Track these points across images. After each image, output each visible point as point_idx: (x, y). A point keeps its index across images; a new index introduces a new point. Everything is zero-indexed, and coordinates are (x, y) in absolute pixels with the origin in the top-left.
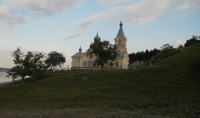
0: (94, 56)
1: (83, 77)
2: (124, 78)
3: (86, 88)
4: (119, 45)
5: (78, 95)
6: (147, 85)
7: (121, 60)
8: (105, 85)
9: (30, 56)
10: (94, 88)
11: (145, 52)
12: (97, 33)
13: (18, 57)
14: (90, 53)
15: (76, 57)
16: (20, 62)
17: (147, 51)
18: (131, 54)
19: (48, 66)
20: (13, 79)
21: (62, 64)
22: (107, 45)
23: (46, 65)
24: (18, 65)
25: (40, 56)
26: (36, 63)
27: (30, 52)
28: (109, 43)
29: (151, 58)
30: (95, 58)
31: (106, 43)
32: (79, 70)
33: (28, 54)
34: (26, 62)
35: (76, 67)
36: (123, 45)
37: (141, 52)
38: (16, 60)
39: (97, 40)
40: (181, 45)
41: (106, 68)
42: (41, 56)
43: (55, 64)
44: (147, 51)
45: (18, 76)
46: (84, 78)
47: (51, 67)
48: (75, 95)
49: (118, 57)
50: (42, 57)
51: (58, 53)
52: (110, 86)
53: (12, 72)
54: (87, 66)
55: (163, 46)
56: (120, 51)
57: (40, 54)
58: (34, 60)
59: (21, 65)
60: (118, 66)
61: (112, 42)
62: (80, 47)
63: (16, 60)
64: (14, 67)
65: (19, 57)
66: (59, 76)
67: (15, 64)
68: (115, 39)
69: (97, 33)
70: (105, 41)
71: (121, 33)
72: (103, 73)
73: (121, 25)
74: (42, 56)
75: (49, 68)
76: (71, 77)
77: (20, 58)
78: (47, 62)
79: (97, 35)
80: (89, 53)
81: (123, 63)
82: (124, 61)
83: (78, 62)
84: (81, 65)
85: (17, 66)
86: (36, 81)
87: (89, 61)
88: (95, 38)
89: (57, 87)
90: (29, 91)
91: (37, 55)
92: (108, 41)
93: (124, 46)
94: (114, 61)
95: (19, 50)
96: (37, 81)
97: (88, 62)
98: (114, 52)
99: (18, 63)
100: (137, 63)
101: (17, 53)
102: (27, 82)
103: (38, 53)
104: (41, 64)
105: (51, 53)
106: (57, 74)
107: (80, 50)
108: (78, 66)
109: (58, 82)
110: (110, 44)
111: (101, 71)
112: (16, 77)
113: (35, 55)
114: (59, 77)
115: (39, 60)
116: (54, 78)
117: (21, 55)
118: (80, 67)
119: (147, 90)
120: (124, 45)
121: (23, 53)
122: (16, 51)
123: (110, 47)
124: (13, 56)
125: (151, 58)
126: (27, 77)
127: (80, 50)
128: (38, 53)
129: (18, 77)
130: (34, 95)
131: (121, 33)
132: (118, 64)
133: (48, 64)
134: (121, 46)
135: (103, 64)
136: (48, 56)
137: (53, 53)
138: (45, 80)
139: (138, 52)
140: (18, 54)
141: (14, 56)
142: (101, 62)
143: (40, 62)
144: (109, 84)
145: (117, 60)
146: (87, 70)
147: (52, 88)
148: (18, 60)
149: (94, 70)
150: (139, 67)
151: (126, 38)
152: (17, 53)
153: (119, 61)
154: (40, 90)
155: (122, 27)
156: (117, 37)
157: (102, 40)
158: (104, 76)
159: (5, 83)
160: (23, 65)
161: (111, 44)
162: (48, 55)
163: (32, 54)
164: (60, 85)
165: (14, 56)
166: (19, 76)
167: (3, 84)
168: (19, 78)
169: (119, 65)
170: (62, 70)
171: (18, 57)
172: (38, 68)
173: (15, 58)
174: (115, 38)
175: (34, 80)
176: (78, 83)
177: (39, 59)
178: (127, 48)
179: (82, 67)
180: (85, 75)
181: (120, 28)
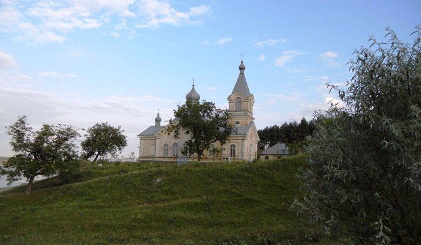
0: (182, 131)
1: (156, 179)
2: (238, 180)
3: (158, 203)
4: (238, 111)
5: (139, 216)
6: (283, 196)
7: (240, 141)
8: (199, 196)
9: (46, 135)
10: (175, 201)
11: (299, 125)
12: (193, 86)
13: (20, 136)
14: (174, 127)
15: (147, 136)
16: (25, 146)
17: (303, 121)
18: (270, 128)
19: (90, 155)
20: (8, 182)
21: (120, 149)
22: (210, 111)
23: (86, 152)
24: (20, 152)
25: (68, 135)
26: (59, 147)
27: (48, 126)
28: (213, 107)
29: (307, 137)
30: (185, 137)
31: (208, 107)
32: (151, 163)
33: (42, 129)
34: (37, 148)
35: (149, 156)
36: (247, 111)
37: (290, 124)
38: (16, 142)
39: (192, 98)
40: (83, 142)
41: (206, 158)
42: (70, 133)
43: (102, 151)
44: (303, 121)
45: (19, 175)
46: (158, 180)
47: (96, 156)
48: (133, 217)
49: (233, 135)
50: (73, 137)
51: (111, 128)
52: (207, 197)
53: (7, 167)
54: (170, 155)
55: (327, 112)
56: (238, 123)
57: (69, 129)
58: (55, 142)
59: (28, 153)
60: (234, 153)
61: (222, 104)
62: (158, 115)
63: (16, 142)
64: (13, 158)
65: (23, 136)
66: (107, 175)
67: (13, 150)
68: (229, 99)
69: (193, 86)
70: (205, 103)
71: (241, 86)
72: (197, 169)
73: (242, 68)
74: (72, 134)
75: (92, 159)
76: (130, 178)
77: (25, 138)
78: (86, 145)
79: (193, 90)
80: (172, 128)
81: (245, 147)
82: (247, 143)
83: (153, 146)
84: (158, 152)
85: (20, 155)
86: (59, 186)
87: (175, 144)
88: (187, 95)
89: (99, 200)
90: (41, 209)
91: (61, 133)
92: (211, 103)
93: (247, 112)
94: (224, 145)
95: (22, 122)
96: (61, 187)
97: (171, 145)
98: (224, 126)
99: (20, 149)
100: (281, 147)
101: (18, 129)
102: (41, 188)
103: (64, 127)
104: (70, 150)
105: (96, 128)
106: (104, 172)
107: (158, 120)
108: (152, 154)
109: (102, 188)
110: (215, 108)
111: (194, 166)
112: (15, 177)
113: (56, 131)
114: (105, 178)
115: (66, 142)
116: (96, 179)
117: (27, 133)
118: (156, 156)
119: (283, 206)
120: (248, 110)
121: (31, 128)
122: (17, 123)
123: (217, 116)
124: (10, 134)
125: (307, 137)
126: (39, 178)
127: (158, 120)
128: (63, 127)
129: (20, 179)
130: (49, 218)
131: (241, 86)
132: (234, 151)
133: (89, 149)
134: (241, 111)
135: (202, 151)
136: (89, 134)
137: (100, 126)
138: (77, 184)
139: (286, 123)
140: (21, 130)
141: (12, 133)
142: (194, 147)
143: (67, 146)
144: (206, 194)
145: (231, 141)
146: (167, 162)
147: (89, 202)
148: (19, 142)
149: (180, 162)
150: (282, 156)
151: (252, 96)
152: (17, 127)
153: (236, 144)
154: (65, 206)
155: (245, 72)
156: (232, 94)
157: (201, 102)
158: (199, 176)
159: (5, 190)
160: (32, 153)
161: (219, 110)
162: (89, 131)
163: (52, 130)
164: (107, 195)
165: (12, 133)
166: (22, 177)
167: (8, 188)
168: (23, 180)
169: (236, 152)
170: (118, 163)
171: (20, 136)
172: (63, 159)
173: (14, 138)
174: (230, 96)
175: (55, 185)
176: (143, 190)
177: (66, 139)
178: (254, 116)
179: (160, 156)
180: (160, 173)
181: (241, 74)
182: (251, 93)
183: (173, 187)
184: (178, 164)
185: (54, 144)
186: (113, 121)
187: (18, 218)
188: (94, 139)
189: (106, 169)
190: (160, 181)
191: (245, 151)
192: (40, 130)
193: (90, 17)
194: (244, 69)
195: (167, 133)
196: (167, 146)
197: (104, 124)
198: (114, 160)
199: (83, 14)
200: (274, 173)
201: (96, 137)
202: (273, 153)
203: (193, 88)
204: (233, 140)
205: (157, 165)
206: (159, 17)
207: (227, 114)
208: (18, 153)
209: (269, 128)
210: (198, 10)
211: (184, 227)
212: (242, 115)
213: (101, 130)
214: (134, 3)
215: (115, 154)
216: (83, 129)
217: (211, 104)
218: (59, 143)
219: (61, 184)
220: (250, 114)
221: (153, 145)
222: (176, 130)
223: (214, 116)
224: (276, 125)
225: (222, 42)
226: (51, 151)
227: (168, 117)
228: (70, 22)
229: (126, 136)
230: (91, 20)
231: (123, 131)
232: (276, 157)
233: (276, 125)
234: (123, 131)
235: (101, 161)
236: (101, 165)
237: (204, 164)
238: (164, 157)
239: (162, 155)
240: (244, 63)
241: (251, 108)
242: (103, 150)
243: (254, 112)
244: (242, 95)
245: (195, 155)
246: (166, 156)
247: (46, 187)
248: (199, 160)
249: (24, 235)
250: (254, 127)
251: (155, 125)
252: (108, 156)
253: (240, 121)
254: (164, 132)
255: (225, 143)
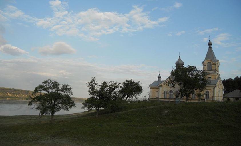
1: (164, 111)
4: (209, 71)
12: (179, 57)
13: (92, 87)
15: (155, 86)
18: (227, 80)
22: (193, 71)
25: (115, 87)
26: (111, 93)
27: (105, 82)
30: (177, 87)
31: (192, 69)
36: (215, 70)
39: (179, 64)
46: (166, 112)
47: (126, 98)
50: (117, 88)
51: (134, 82)
54: (168, 97)
56: (210, 78)
57: (115, 84)
59: (96, 96)
60: (208, 96)
61: (200, 67)
62: (159, 74)
64: (89, 98)
68: (203, 63)
69: (179, 57)
71: (210, 55)
74: (117, 86)
78: (121, 91)
79: (179, 59)
80: (170, 82)
82: (216, 90)
87: (171, 91)
91: (111, 85)
92: (194, 67)
93: (216, 71)
94: (202, 91)
95: (94, 80)
98: (202, 80)
105: (126, 82)
107: (159, 77)
108: (157, 96)
113: (109, 85)
117: (96, 86)
118: (160, 97)
120: (216, 70)
122: (91, 81)
123: (197, 74)
124: (88, 87)
127: (159, 77)
128: (113, 83)
131: (210, 55)
134: (211, 70)
136: (123, 86)
137: (128, 81)
138: (120, 113)
139: (237, 76)
140: (93, 84)
145: (207, 89)
146: (168, 101)
148: (92, 91)
151: (218, 61)
152: (92, 83)
153: (209, 91)
155: (212, 46)
161: (198, 70)
171: (92, 87)
174: (203, 62)
177: (114, 89)
178: (220, 73)
179: (162, 98)
182: (217, 59)
183: (175, 116)
185: (108, 91)
186: (135, 79)
187: (94, 129)
188: (125, 89)
190: (167, 113)
191: (216, 95)
192: (101, 84)
193: (109, 29)
194: (211, 44)
197: (130, 80)
199: (106, 28)
202: (233, 96)
203: (180, 58)
204: (208, 89)
206: (142, 25)
207: (204, 72)
208: (92, 96)
209: (225, 80)
210: (162, 20)
211: (188, 141)
214: (129, 20)
217: (194, 67)
218: (111, 90)
219: (111, 113)
221: (157, 91)
223: (195, 74)
224: (230, 78)
225: (179, 34)
226: (107, 94)
227: (166, 75)
228: (100, 32)
230: (110, 30)
232: (235, 99)
233: (230, 78)
240: (211, 41)
241: (218, 68)
242: (130, 94)
243: (219, 71)
244: (211, 60)
245: (185, 97)
246: (165, 98)
247: (104, 114)
248: (187, 100)
249: (100, 138)
251: (157, 80)
252: (133, 98)
253: (211, 76)
254: (166, 84)
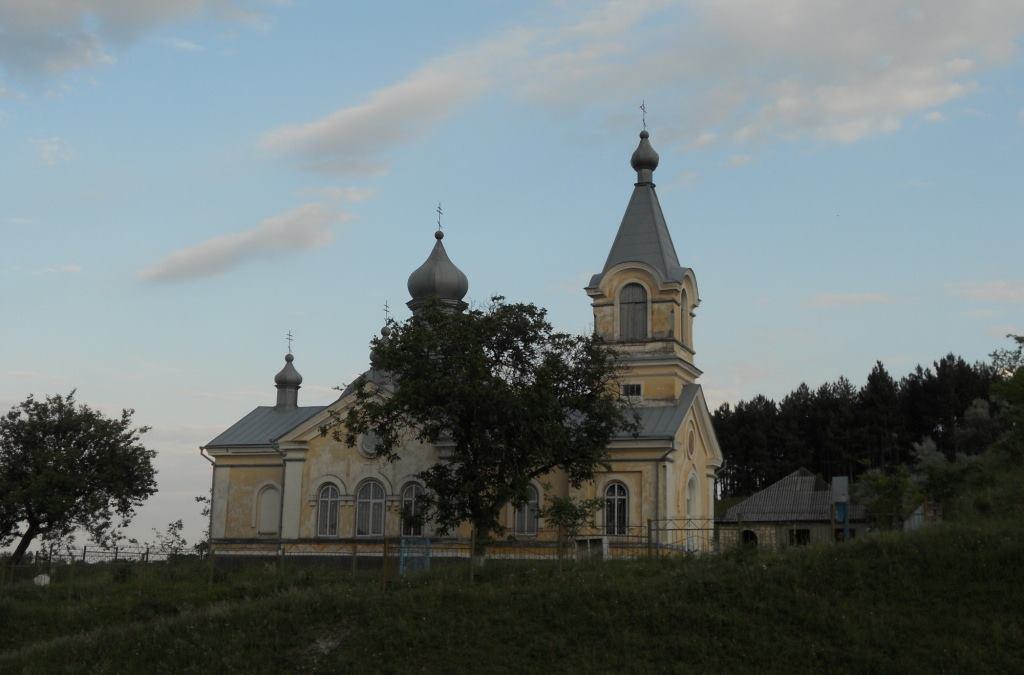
1: (313, 641)
4: (633, 342)
7: (648, 469)
11: (862, 394)
12: (439, 236)
15: (249, 450)
17: (879, 378)
18: (739, 409)
21: (124, 508)
22: (527, 341)
29: (916, 445)
30: (417, 452)
35: (251, 535)
36: (669, 338)
37: (823, 391)
39: (435, 290)
44: (879, 378)
46: (323, 646)
47: (18, 541)
51: (88, 417)
54: (346, 530)
56: (634, 390)
68: (594, 289)
69: (439, 236)
71: (642, 231)
73: (644, 162)
76: (196, 636)
79: (438, 254)
80: (366, 415)
82: (674, 476)
87: (369, 486)
92: (531, 310)
93: (672, 347)
94: (585, 483)
98: (584, 404)
105: (24, 417)
107: (288, 383)
108: (267, 525)
110: (549, 328)
118: (285, 536)
120: (677, 336)
123: (553, 361)
125: (916, 445)
127: (288, 383)
131: (642, 231)
134: (644, 342)
135: (494, 511)
137: (42, 410)
139: (803, 386)
145: (615, 466)
151: (688, 276)
153: (630, 481)
155: (657, 176)
161: (560, 336)
170: (122, 570)
174: (596, 280)
178: (697, 361)
179: (303, 535)
184: (402, 570)
189: (75, 597)
194: (441, 238)
195: (343, 438)
196: (335, 492)
198: (96, 555)
200: (833, 604)
201: (23, 459)
202: (774, 518)
203: (439, 245)
205: (301, 574)
209: (732, 409)
212: (653, 357)
213: (47, 428)
215: (108, 532)
216: (642, 107)
217: (532, 314)
220: (682, 354)
221: (270, 487)
222: (382, 426)
223: (539, 361)
227: (334, 369)
229: (154, 454)
231: (144, 430)
233: (761, 398)
234: (144, 430)
235: (45, 563)
236: (44, 580)
237: (522, 568)
238: (318, 541)
239: (310, 530)
240: (652, 141)
244: (645, 272)
246: (328, 535)
248: (478, 550)
250: (702, 404)
251: (272, 402)
252: (80, 542)
255: (589, 476)
